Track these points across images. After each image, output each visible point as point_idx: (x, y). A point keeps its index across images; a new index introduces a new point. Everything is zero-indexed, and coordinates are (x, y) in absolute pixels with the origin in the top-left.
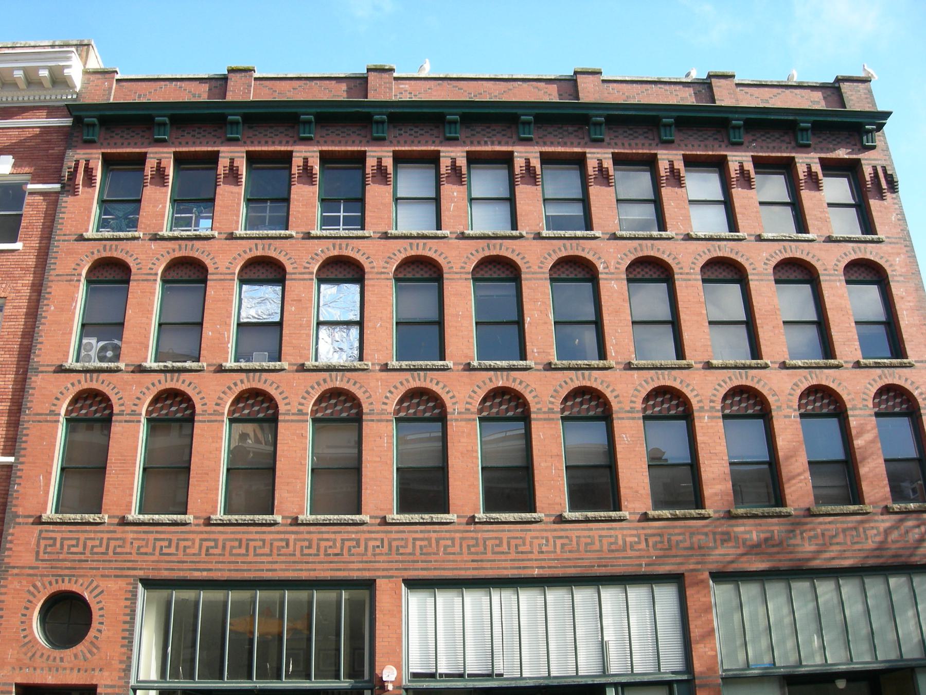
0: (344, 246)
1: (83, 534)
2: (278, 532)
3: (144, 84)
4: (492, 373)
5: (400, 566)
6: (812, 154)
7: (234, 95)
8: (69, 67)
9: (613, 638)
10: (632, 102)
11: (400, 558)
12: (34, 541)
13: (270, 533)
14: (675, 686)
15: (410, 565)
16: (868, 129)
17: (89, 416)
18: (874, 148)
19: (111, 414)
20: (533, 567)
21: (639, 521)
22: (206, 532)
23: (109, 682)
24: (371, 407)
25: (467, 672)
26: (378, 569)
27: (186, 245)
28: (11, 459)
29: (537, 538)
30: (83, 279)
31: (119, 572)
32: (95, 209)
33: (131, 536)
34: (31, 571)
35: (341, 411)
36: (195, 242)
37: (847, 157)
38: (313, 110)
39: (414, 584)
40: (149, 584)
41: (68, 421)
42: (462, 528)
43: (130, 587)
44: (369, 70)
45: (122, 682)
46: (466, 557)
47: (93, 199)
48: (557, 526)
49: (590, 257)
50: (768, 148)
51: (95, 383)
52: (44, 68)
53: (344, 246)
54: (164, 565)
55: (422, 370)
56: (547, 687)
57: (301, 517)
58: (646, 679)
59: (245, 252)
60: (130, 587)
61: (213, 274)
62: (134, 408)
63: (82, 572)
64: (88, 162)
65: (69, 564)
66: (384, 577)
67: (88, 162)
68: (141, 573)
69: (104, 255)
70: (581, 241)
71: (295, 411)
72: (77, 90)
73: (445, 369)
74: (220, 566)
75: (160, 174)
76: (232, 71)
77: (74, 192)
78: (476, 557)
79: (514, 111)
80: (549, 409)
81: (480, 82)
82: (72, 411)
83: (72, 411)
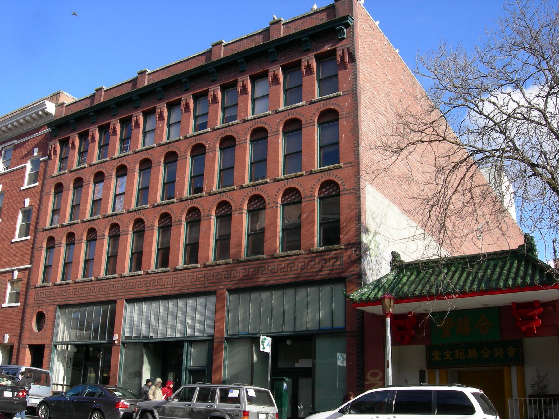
0: (325, 104)
1: (112, 282)
2: (93, 284)
3: (72, 105)
4: (162, 207)
5: (124, 294)
6: (311, 54)
7: (274, 37)
8: (46, 108)
9: (190, 321)
10: (235, 53)
11: (125, 290)
12: (34, 294)
13: (91, 284)
14: (69, 346)
15: (127, 293)
16: (338, 29)
17: (225, 214)
18: (344, 38)
19: (340, 192)
20: (164, 291)
21: (203, 267)
22: (75, 286)
23: (48, 343)
24: (344, 187)
25: (133, 336)
26: (118, 296)
27: (327, 103)
28: (31, 266)
29: (167, 278)
30: (316, 124)
31: (53, 303)
32: (282, 96)
33: (57, 290)
34: (32, 305)
35: (332, 192)
36: (81, 170)
37: (329, 49)
38: (213, 66)
39: (130, 301)
40: (61, 307)
41: (320, 199)
42: (144, 276)
43: (55, 309)
44: (139, 74)
45: (51, 343)
46: (144, 289)
47: (314, 80)
48: (204, 269)
49: (262, 125)
50: (289, 58)
51: (224, 198)
52: (40, 111)
53: (325, 104)
54: (64, 300)
55: (327, 171)
56: (164, 342)
57: (56, 283)
58: (200, 338)
59: (281, 120)
60: (55, 309)
61: (180, 157)
62: (240, 207)
63: (44, 304)
64: (348, 49)
65: (41, 302)
66: (120, 299)
67: (348, 49)
68: (57, 303)
69: (288, 118)
70: (201, 135)
71: (101, 235)
72: (54, 115)
73: (234, 190)
74: (77, 298)
75: (309, 68)
76: (97, 90)
77: (345, 67)
78: (147, 288)
79: (129, 96)
80: (240, 208)
81: (177, 65)
82: (284, 201)
83: (284, 201)
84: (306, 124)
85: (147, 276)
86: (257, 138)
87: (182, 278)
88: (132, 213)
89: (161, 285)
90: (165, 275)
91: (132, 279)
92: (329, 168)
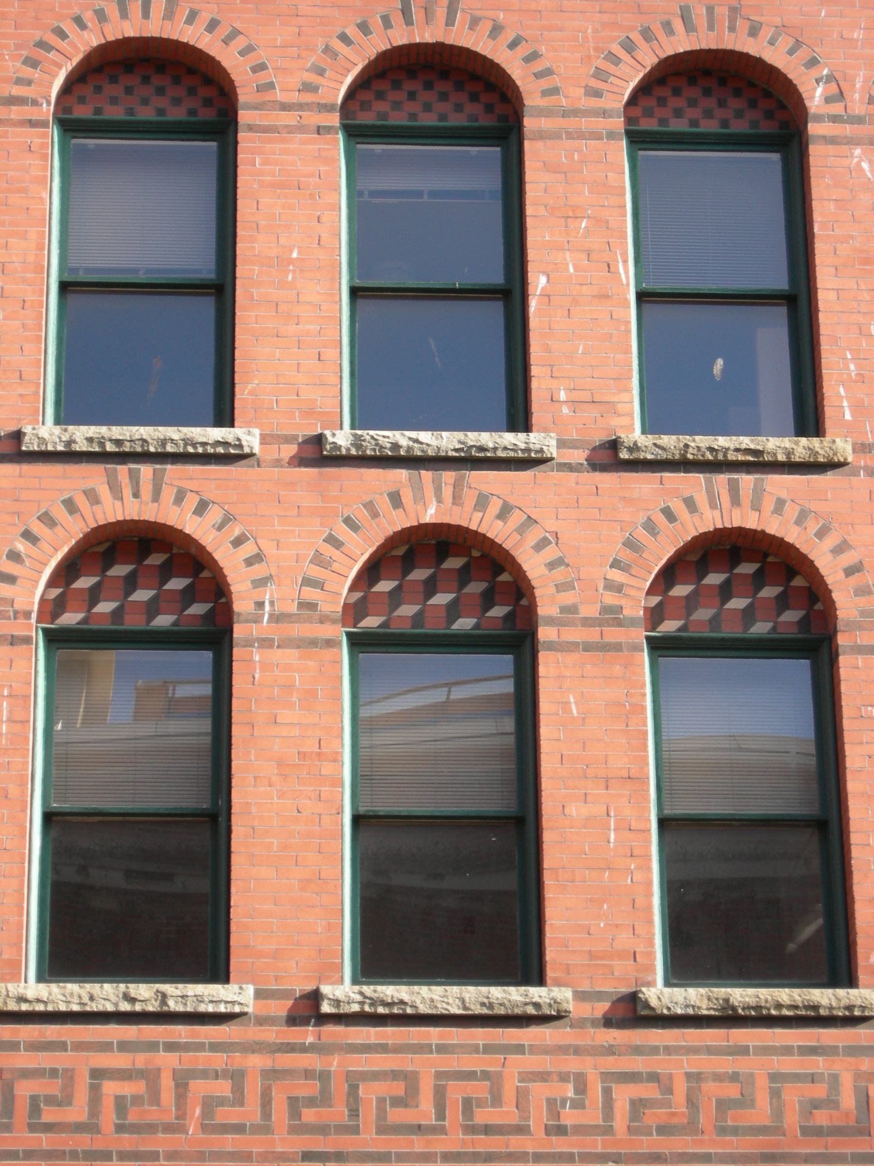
4: (402, 474)
17: (430, 628)
24: (568, 598)
29: (543, 1077)
35: (152, 608)
42: (271, 1034)
84: (835, 119)
85: (309, 1034)
86: (115, 113)
87: (711, 1089)
88: (58, 469)
89: (487, 1130)
90: (519, 1049)
91: (124, 1046)
92: (187, 441)
